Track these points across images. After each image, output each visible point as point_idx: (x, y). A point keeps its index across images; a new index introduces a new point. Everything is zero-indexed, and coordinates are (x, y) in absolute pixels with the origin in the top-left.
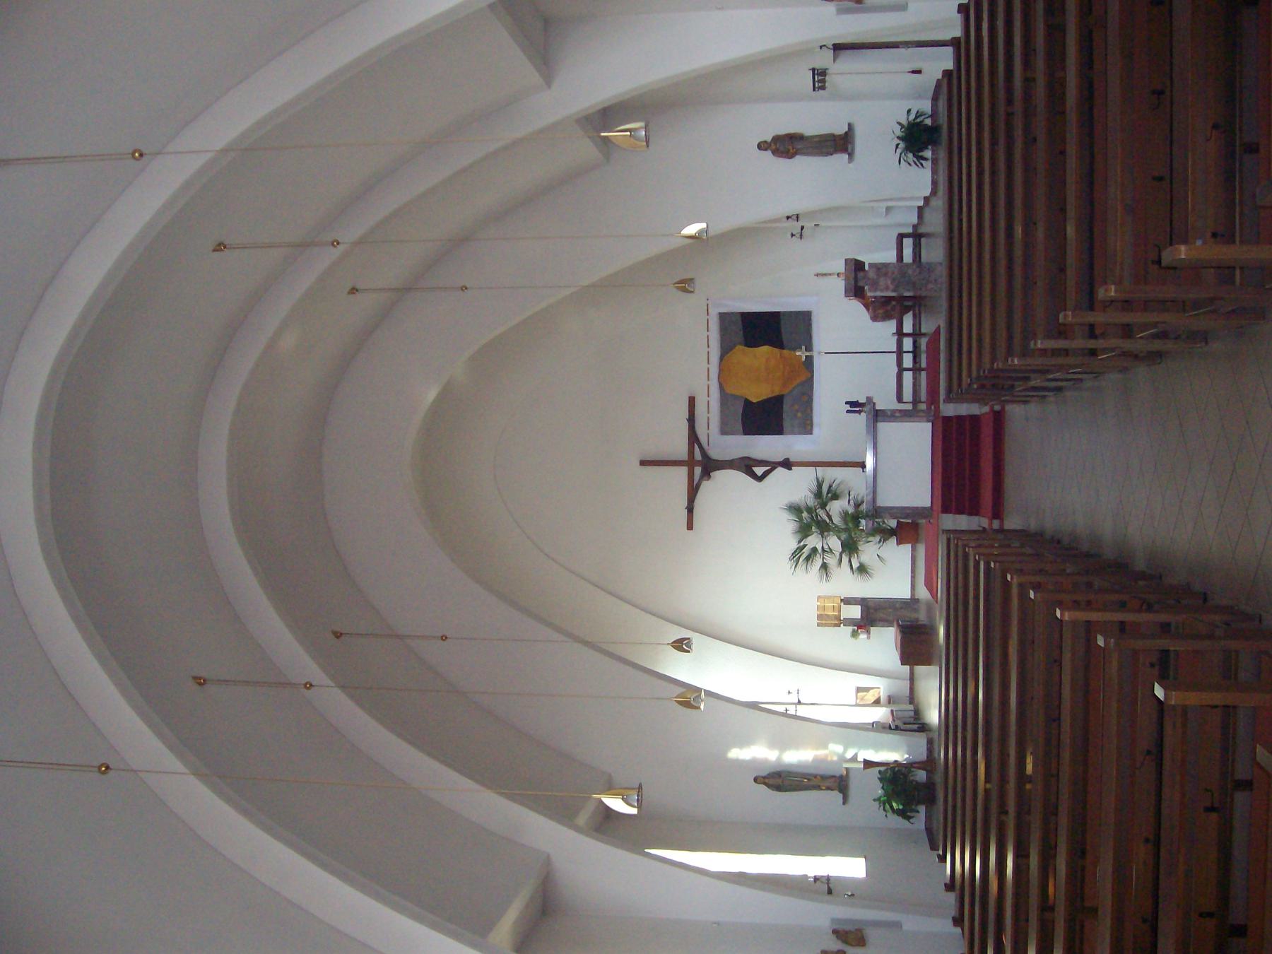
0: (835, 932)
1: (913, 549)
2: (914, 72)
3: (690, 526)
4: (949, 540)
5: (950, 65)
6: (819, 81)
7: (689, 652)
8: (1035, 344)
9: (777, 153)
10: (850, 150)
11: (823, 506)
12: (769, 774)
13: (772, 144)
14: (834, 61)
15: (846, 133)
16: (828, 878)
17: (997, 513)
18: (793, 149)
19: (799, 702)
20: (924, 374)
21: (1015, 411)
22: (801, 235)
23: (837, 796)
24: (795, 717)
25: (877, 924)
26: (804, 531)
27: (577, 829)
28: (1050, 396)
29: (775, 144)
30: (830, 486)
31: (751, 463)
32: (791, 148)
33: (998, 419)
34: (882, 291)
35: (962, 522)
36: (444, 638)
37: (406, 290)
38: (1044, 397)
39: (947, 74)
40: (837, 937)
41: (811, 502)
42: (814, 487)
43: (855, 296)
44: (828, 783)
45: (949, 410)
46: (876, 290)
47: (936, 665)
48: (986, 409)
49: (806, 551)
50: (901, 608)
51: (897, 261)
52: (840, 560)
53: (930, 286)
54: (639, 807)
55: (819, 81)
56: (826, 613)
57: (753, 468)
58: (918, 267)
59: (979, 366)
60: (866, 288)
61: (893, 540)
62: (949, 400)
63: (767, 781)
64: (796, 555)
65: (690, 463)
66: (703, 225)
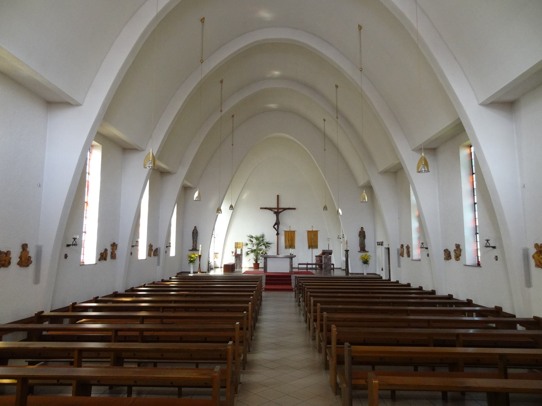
0: (157, 249)
1: (252, 268)
2: (382, 269)
3: (261, 208)
4: (260, 277)
5: (384, 278)
9: (360, 232)
11: (264, 244)
12: (197, 230)
14: (385, 248)
16: (170, 246)
17: (266, 290)
20: (306, 270)
21: (293, 294)
26: (257, 239)
27: (183, 181)
33: (291, 290)
34: (324, 259)
35: (264, 281)
36: (233, 145)
37: (325, 135)
39: (381, 278)
42: (269, 242)
45: (293, 277)
47: (224, 274)
49: (252, 239)
52: (249, 249)
54: (195, 200)
60: (325, 256)
62: (296, 277)
65: (278, 208)
66: (341, 214)
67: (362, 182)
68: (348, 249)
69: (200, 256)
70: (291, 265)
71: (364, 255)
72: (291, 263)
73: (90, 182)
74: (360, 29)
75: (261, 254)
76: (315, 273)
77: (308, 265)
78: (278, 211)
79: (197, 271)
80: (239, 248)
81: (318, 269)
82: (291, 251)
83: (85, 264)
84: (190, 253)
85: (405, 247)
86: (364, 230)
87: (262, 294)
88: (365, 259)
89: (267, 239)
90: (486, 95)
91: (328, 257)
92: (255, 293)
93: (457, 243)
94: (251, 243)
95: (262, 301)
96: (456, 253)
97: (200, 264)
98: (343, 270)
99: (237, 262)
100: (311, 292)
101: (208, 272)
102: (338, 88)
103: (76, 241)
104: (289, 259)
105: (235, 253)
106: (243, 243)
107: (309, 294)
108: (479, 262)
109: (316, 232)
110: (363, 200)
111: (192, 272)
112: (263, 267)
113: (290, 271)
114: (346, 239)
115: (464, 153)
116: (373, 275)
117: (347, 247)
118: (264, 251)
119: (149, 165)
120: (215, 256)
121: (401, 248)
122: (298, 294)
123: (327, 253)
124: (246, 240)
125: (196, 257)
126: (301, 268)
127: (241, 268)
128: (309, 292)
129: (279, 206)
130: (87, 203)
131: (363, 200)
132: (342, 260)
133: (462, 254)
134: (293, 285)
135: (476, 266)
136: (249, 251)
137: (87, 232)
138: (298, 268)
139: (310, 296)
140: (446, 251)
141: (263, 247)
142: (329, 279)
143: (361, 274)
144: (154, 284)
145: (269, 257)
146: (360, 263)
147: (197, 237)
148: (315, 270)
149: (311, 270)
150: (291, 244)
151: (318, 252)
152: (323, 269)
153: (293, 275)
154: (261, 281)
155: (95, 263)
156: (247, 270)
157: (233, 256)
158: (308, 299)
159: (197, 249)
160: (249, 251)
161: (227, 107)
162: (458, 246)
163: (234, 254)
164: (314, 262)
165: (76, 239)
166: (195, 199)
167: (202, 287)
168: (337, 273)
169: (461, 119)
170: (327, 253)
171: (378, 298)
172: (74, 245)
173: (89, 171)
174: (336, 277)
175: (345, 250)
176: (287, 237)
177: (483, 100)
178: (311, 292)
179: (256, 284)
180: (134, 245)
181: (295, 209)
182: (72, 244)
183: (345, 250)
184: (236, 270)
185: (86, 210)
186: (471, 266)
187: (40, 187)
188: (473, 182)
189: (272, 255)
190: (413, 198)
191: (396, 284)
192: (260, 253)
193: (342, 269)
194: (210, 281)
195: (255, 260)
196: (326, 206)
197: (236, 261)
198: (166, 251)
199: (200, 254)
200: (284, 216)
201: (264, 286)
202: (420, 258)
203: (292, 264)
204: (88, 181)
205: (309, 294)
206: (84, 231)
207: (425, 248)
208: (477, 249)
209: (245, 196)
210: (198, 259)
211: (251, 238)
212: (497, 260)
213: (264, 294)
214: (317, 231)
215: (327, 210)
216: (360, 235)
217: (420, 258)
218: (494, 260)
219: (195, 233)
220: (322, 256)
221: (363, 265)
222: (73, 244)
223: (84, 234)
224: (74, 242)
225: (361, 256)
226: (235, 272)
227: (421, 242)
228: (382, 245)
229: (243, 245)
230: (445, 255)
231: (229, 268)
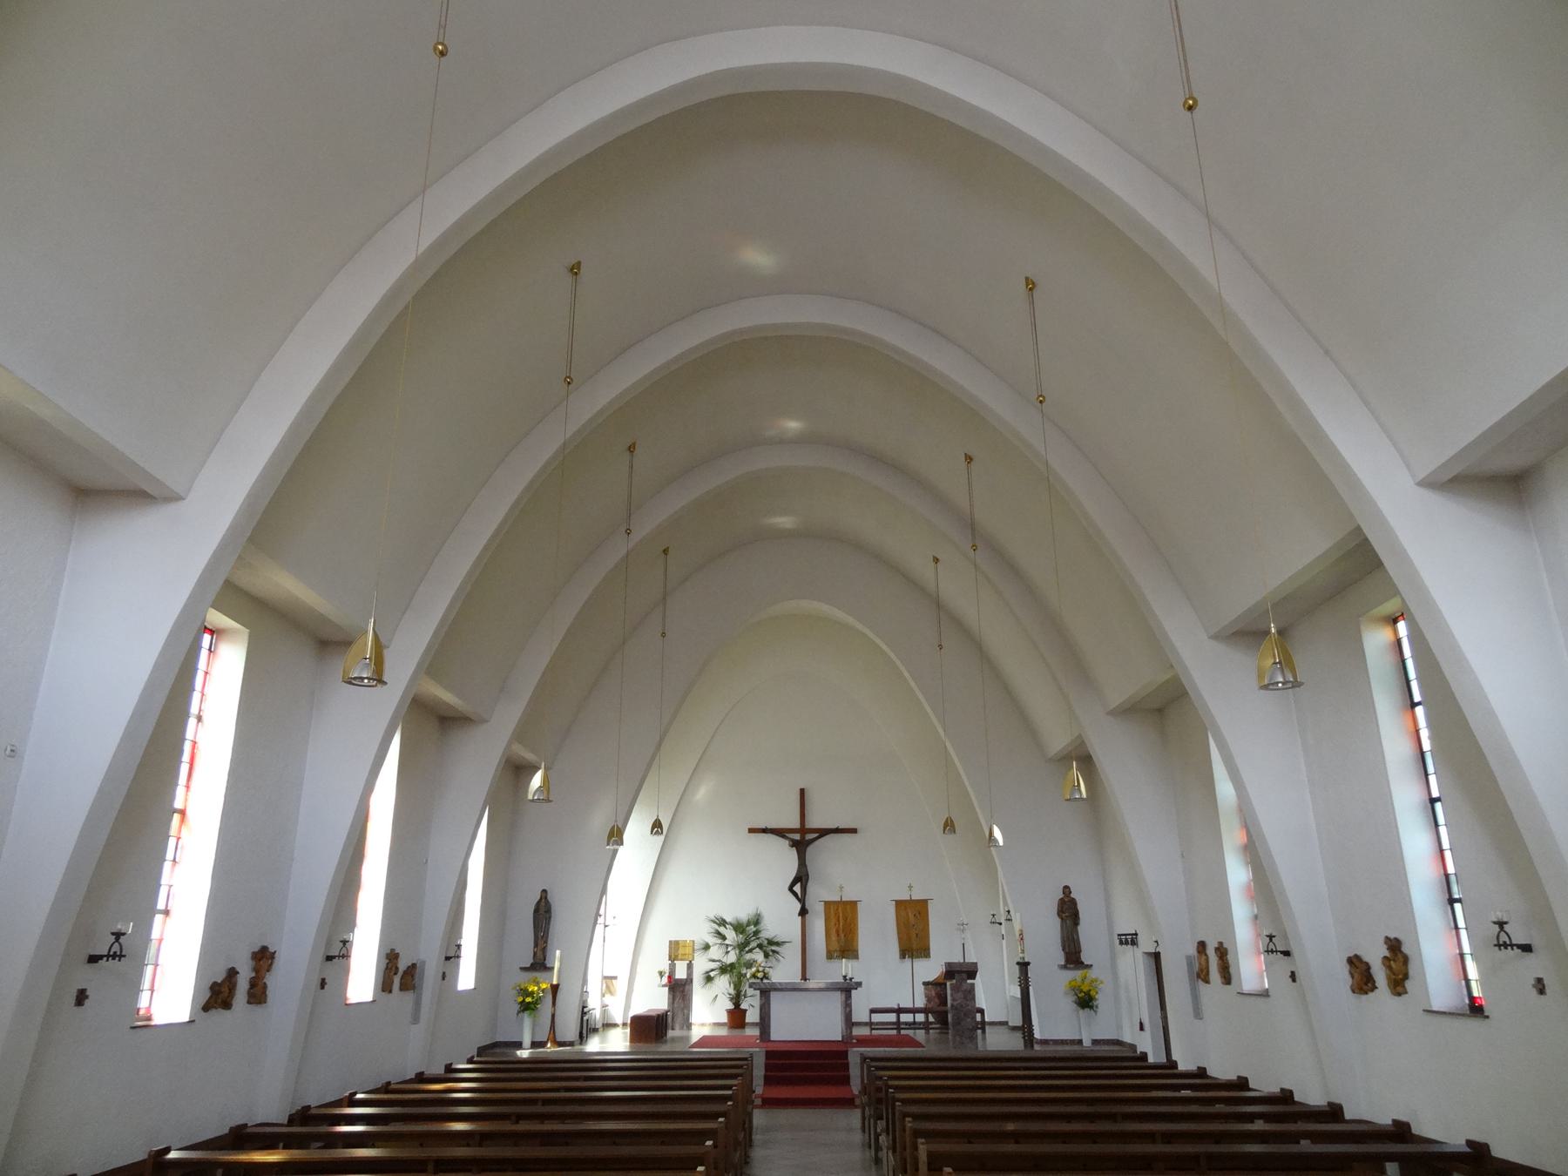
0: (414, 966)
2: (1141, 1024)
3: (752, 831)
4: (745, 1059)
6: (1126, 939)
7: (652, 832)
9: (1062, 902)
10: (1068, 966)
11: (760, 946)
14: (1146, 953)
15: (1082, 963)
16: (459, 957)
17: (768, 1103)
19: (606, 926)
21: (854, 1118)
23: (528, 963)
24: (595, 923)
25: (418, 1004)
26: (739, 928)
29: (1069, 901)
30: (777, 953)
33: (848, 1103)
34: (952, 995)
35: (759, 1072)
36: (663, 635)
37: (938, 604)
39: (1144, 1056)
40: (409, 967)
41: (765, 935)
44: (539, 954)
46: (952, 989)
47: (631, 1047)
48: (856, 1092)
49: (722, 929)
52: (714, 961)
53: (958, 1039)
54: (533, 801)
55: (1126, 939)
59: (897, 1088)
60: (954, 981)
61: (731, 1006)
62: (864, 1059)
64: (722, 922)
65: (803, 830)
66: (1001, 843)
67: (1058, 740)
68: (1026, 960)
69: (555, 989)
70: (848, 1016)
71: (1079, 980)
72: (845, 1008)
73: (200, 745)
74: (1030, 289)
75: (750, 978)
76: (928, 1043)
77: (901, 1015)
78: (804, 838)
79: (546, 1040)
80: (681, 960)
81: (933, 1028)
82: (846, 967)
83: (153, 1023)
84: (523, 979)
85: (1211, 952)
86: (1072, 895)
87: (751, 1122)
88: (1081, 991)
89: (770, 929)
90: (1433, 459)
91: (964, 987)
92: (722, 1125)
93: (1392, 936)
94: (720, 941)
95: (751, 1146)
96: (1389, 968)
97: (553, 1016)
98: (1014, 1029)
99: (676, 1006)
100: (916, 1117)
101: (581, 1044)
102: (972, 463)
103: (120, 944)
104: (838, 994)
105: (669, 977)
106: (693, 941)
107: (911, 1127)
108: (1472, 999)
109: (923, 903)
110: (1072, 793)
111: (527, 1041)
112: (758, 1021)
113: (843, 1037)
114: (1017, 925)
115: (1376, 640)
116: (1106, 1048)
117: (1023, 951)
118: (761, 969)
119: (362, 670)
120: (608, 987)
121: (1199, 952)
122: (872, 1120)
123: (961, 973)
124: (704, 934)
125: (543, 991)
126: (878, 1024)
127: (689, 1026)
128: (910, 1119)
129: (806, 823)
130: (183, 813)
131: (1072, 793)
132: (1008, 998)
133: (1411, 973)
134: (856, 1086)
135: (1463, 1015)
136: (712, 970)
137: (172, 913)
138: (870, 1024)
139: (905, 1115)
140: (1357, 964)
141: (758, 956)
142: (982, 1064)
143: (1072, 1042)
144: (387, 1092)
145: (776, 990)
146: (1067, 1004)
147: (549, 924)
148: (923, 1031)
149: (912, 1031)
150: (844, 944)
151: (931, 969)
152: (950, 1026)
153: (855, 1049)
154: (750, 1068)
155: (187, 1020)
156: (707, 1031)
157: (664, 986)
158: (908, 1144)
159: (548, 966)
160: (712, 970)
161: (645, 526)
162: (1394, 946)
163: (665, 980)
164: (920, 1002)
165: (124, 934)
166: (530, 797)
167: (546, 1102)
168: (997, 1042)
169: (1365, 531)
170: (961, 973)
171: (1150, 1137)
172: (114, 956)
173: (200, 710)
174: (991, 1055)
175: (1018, 963)
176: (833, 921)
177: (1432, 467)
178: (916, 1117)
179: (729, 1087)
180: (337, 955)
181: (854, 831)
182: (337, 954)
183: (1018, 963)
184: (670, 1033)
185: (178, 839)
186: (1450, 1013)
187: (13, 757)
188: (1417, 731)
189: (785, 983)
190: (1225, 789)
191: (1198, 1081)
192: (748, 976)
193: (1010, 1024)
194: (577, 1079)
195: (731, 999)
196: (952, 821)
197: (673, 1003)
198: (444, 973)
199: (555, 982)
200: (824, 855)
201: (759, 1088)
202: (1267, 986)
203: (851, 1011)
204: (194, 743)
205: (910, 1125)
206: (161, 905)
207: (1282, 952)
208: (1462, 955)
209: (702, 793)
210: (550, 997)
211: (719, 925)
212: (1542, 991)
213: (759, 1118)
214: (925, 902)
215: (953, 831)
216: (1063, 913)
217: (1267, 986)
218: (1534, 992)
219: (543, 913)
220: (945, 985)
221: (1078, 1012)
222: (111, 953)
223: (158, 918)
224: (116, 948)
225: (1070, 983)
226: (666, 1041)
227: (1266, 932)
228: (1134, 943)
229: (694, 950)
230: (1353, 977)
231: (648, 1028)
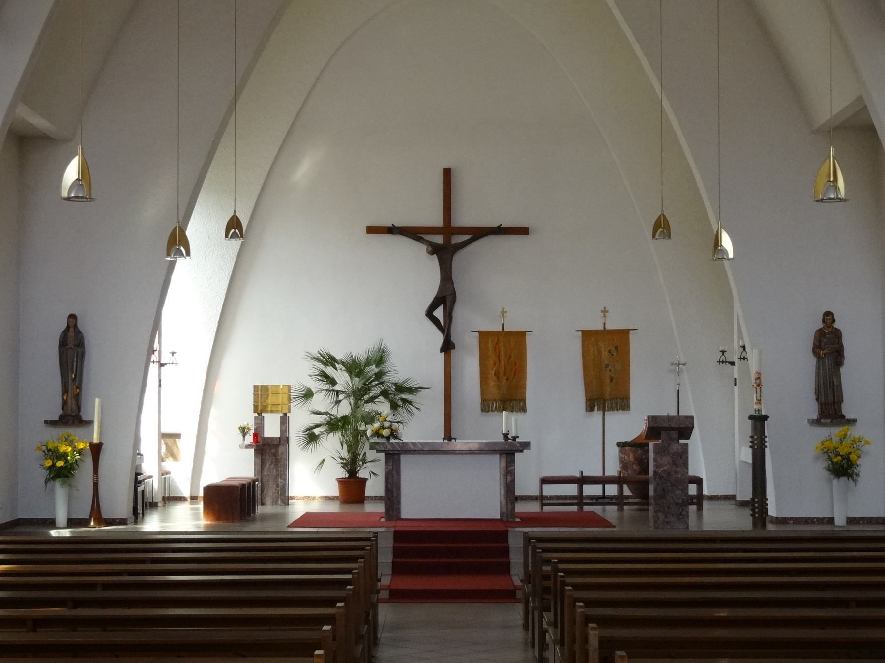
3: (371, 230)
7: (226, 236)
8: (592, 628)
10: (822, 421)
12: (80, 332)
13: (830, 330)
17: (397, 596)
18: (825, 354)
19: (162, 365)
21: (515, 614)
22: (723, 362)
23: (55, 413)
24: (148, 362)
26: (354, 368)
28: (534, 652)
31: (449, 303)
32: (826, 351)
33: (507, 595)
35: (385, 558)
38: (533, 646)
43: (648, 428)
44: (71, 403)
45: (516, 539)
49: (329, 370)
50: (278, 486)
51: (690, 477)
52: (319, 413)
53: (661, 516)
56: (270, 395)
57: (442, 306)
58: (683, 501)
62: (528, 539)
63: (72, 330)
65: (448, 229)
66: (731, 256)
